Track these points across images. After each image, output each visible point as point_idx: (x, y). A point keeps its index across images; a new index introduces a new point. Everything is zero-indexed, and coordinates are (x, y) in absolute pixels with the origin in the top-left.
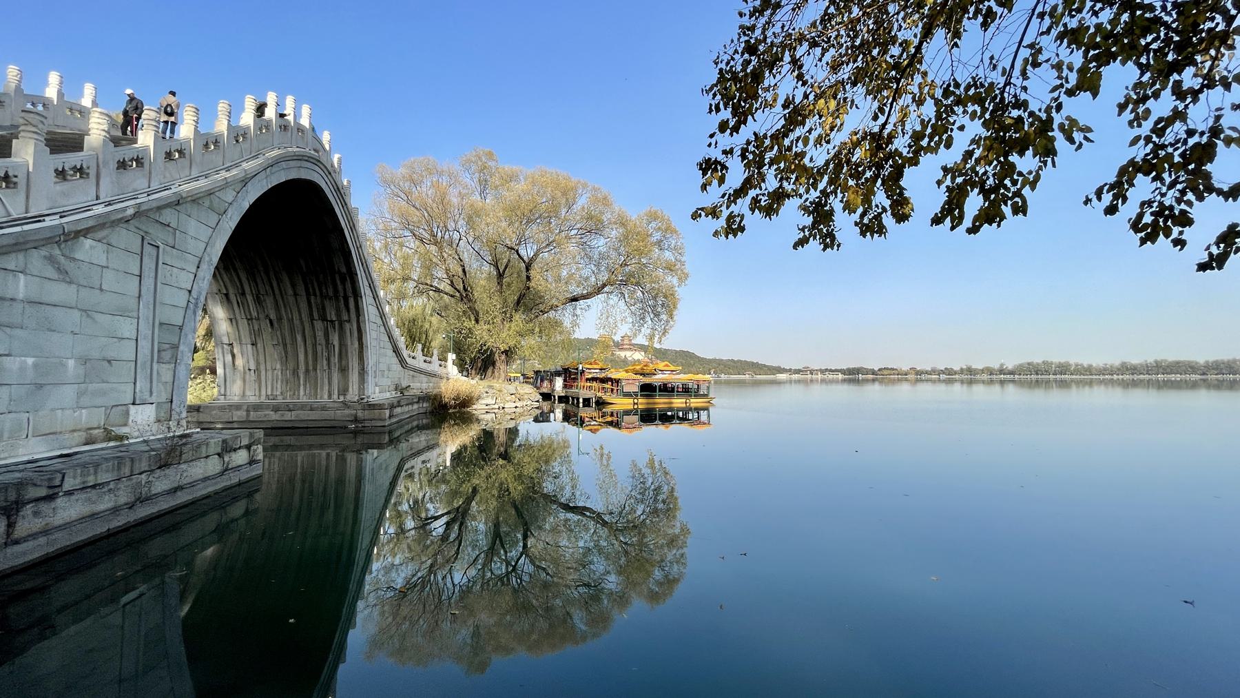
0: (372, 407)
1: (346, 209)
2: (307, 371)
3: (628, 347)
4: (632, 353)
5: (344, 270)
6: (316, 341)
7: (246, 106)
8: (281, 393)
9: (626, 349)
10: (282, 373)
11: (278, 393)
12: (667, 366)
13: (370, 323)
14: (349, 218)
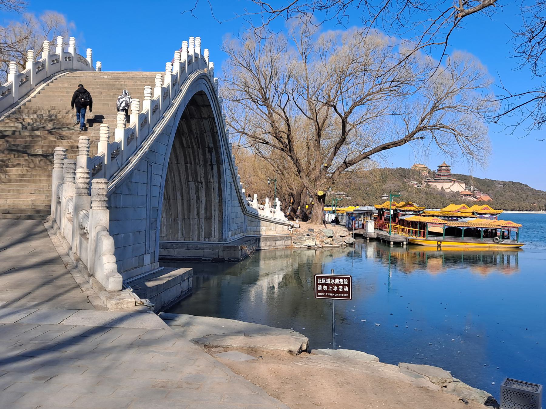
0: (228, 248)
1: (216, 102)
2: (183, 219)
3: (446, 178)
4: (451, 184)
5: (211, 145)
6: (190, 197)
7: (175, 58)
8: (166, 235)
9: (444, 180)
10: (166, 220)
11: (164, 235)
12: (486, 209)
13: (227, 183)
14: (218, 108)
